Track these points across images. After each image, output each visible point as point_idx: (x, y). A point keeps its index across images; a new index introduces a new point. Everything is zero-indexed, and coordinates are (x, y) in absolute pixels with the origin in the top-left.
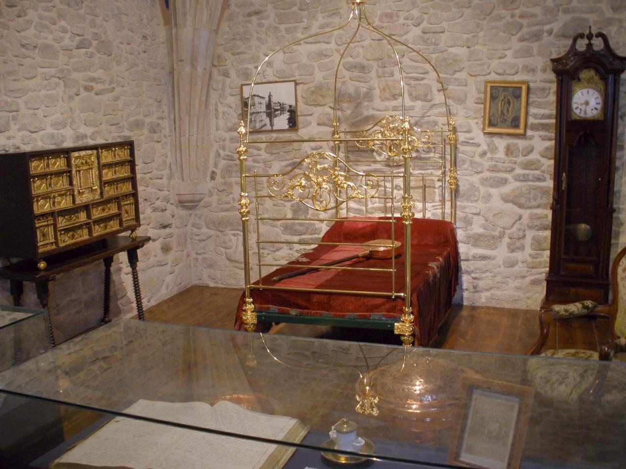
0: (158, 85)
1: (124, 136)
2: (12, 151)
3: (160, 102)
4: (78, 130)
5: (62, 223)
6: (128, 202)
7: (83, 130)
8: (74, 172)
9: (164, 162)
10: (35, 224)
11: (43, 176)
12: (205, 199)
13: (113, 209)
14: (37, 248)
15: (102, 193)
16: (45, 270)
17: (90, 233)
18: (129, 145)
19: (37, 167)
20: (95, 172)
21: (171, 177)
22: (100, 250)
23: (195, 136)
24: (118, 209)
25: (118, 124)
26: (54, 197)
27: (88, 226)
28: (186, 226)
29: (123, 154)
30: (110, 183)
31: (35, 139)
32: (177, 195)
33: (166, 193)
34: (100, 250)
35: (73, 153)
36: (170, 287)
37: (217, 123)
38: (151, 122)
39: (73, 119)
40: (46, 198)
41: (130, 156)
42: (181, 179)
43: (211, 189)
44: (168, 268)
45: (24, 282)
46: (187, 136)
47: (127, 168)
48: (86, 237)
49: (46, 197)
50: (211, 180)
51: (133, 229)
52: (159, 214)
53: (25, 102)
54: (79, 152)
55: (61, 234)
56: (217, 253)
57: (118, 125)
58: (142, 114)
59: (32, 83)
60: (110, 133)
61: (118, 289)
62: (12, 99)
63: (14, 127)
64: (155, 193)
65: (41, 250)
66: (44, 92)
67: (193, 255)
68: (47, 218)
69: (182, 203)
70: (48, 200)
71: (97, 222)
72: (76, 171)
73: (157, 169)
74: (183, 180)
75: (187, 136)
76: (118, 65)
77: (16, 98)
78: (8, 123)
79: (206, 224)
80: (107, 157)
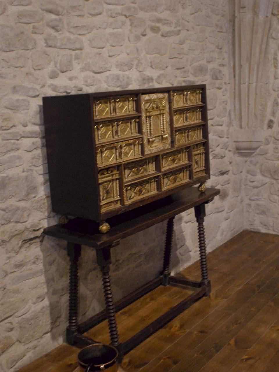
0: (219, 32)
1: (189, 81)
2: (73, 93)
3: (221, 49)
4: (145, 73)
5: (129, 176)
6: (199, 152)
7: (149, 72)
8: (143, 118)
9: (225, 109)
10: (98, 179)
11: (108, 122)
12: (262, 147)
13: (183, 160)
14: (99, 207)
15: (173, 142)
16: (108, 232)
17: (159, 187)
18: (202, 89)
19: (102, 111)
20: (166, 118)
21: (230, 124)
22: (165, 206)
23: (254, 84)
24: (189, 160)
25: (184, 68)
26: (121, 147)
27: (157, 180)
28: (241, 172)
29: (194, 99)
30: (181, 130)
31: (100, 81)
32: (235, 142)
33: (225, 140)
34: (165, 206)
35: (144, 96)
36: (225, 233)
37: (276, 72)
38: (214, 69)
39: (139, 60)
40: (112, 148)
41: (202, 101)
42: (239, 126)
43: (267, 137)
44: (224, 214)
45: (83, 246)
46: (247, 84)
47: (199, 114)
48: (154, 192)
49: (111, 146)
50: (268, 129)
51: (202, 181)
52: (218, 160)
53: (89, 40)
54: (150, 95)
55: (127, 190)
56: (271, 201)
57: (183, 70)
58: (205, 60)
59: (97, 20)
60: (176, 77)
61: (178, 239)
62: (76, 36)
63: (77, 66)
64: (216, 140)
65: (103, 210)
66: (109, 30)
67: (247, 201)
68: (112, 172)
69: (239, 150)
70: (114, 150)
71: (167, 174)
72: (146, 117)
73: (218, 116)
74: (241, 127)
75: (247, 84)
76: (183, 8)
77: (80, 35)
78: (70, 61)
79: (261, 172)
80: (179, 102)
